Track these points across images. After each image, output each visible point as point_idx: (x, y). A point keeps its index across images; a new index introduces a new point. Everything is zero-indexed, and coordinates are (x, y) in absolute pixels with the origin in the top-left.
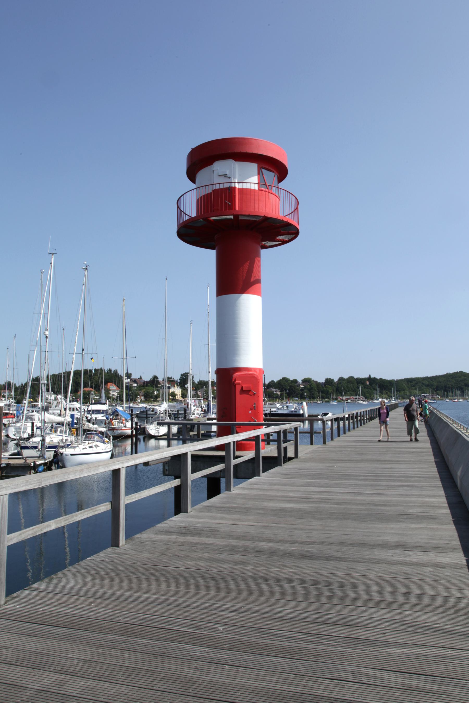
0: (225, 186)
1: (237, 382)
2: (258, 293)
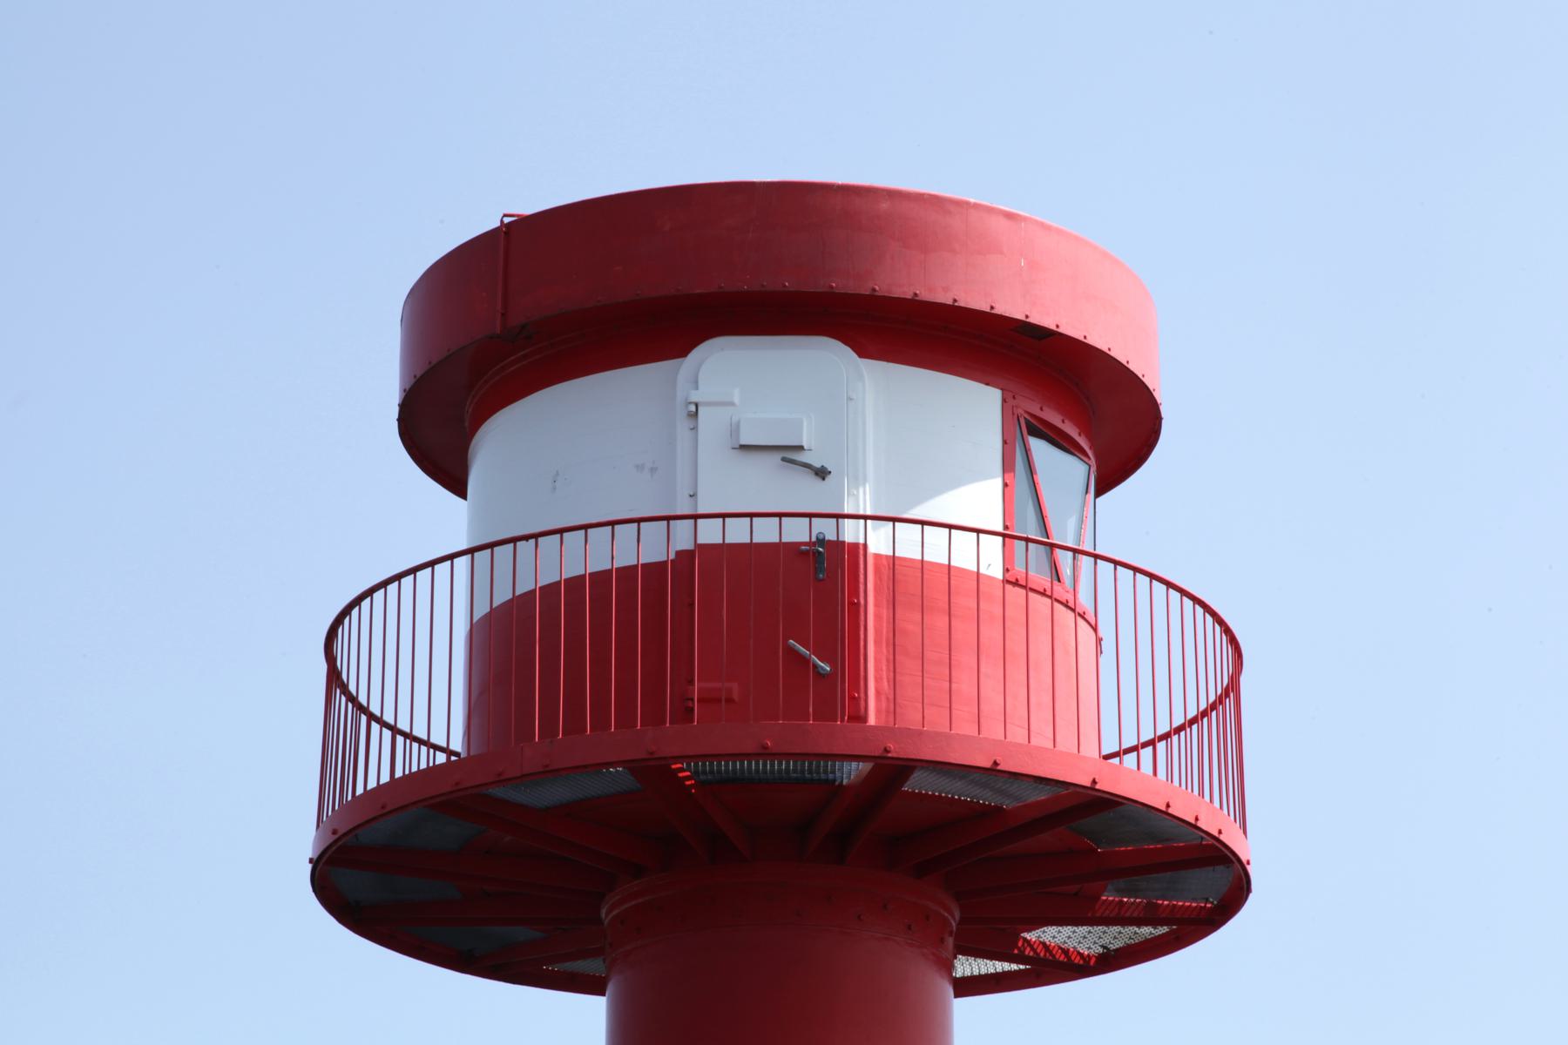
0: (796, 532)
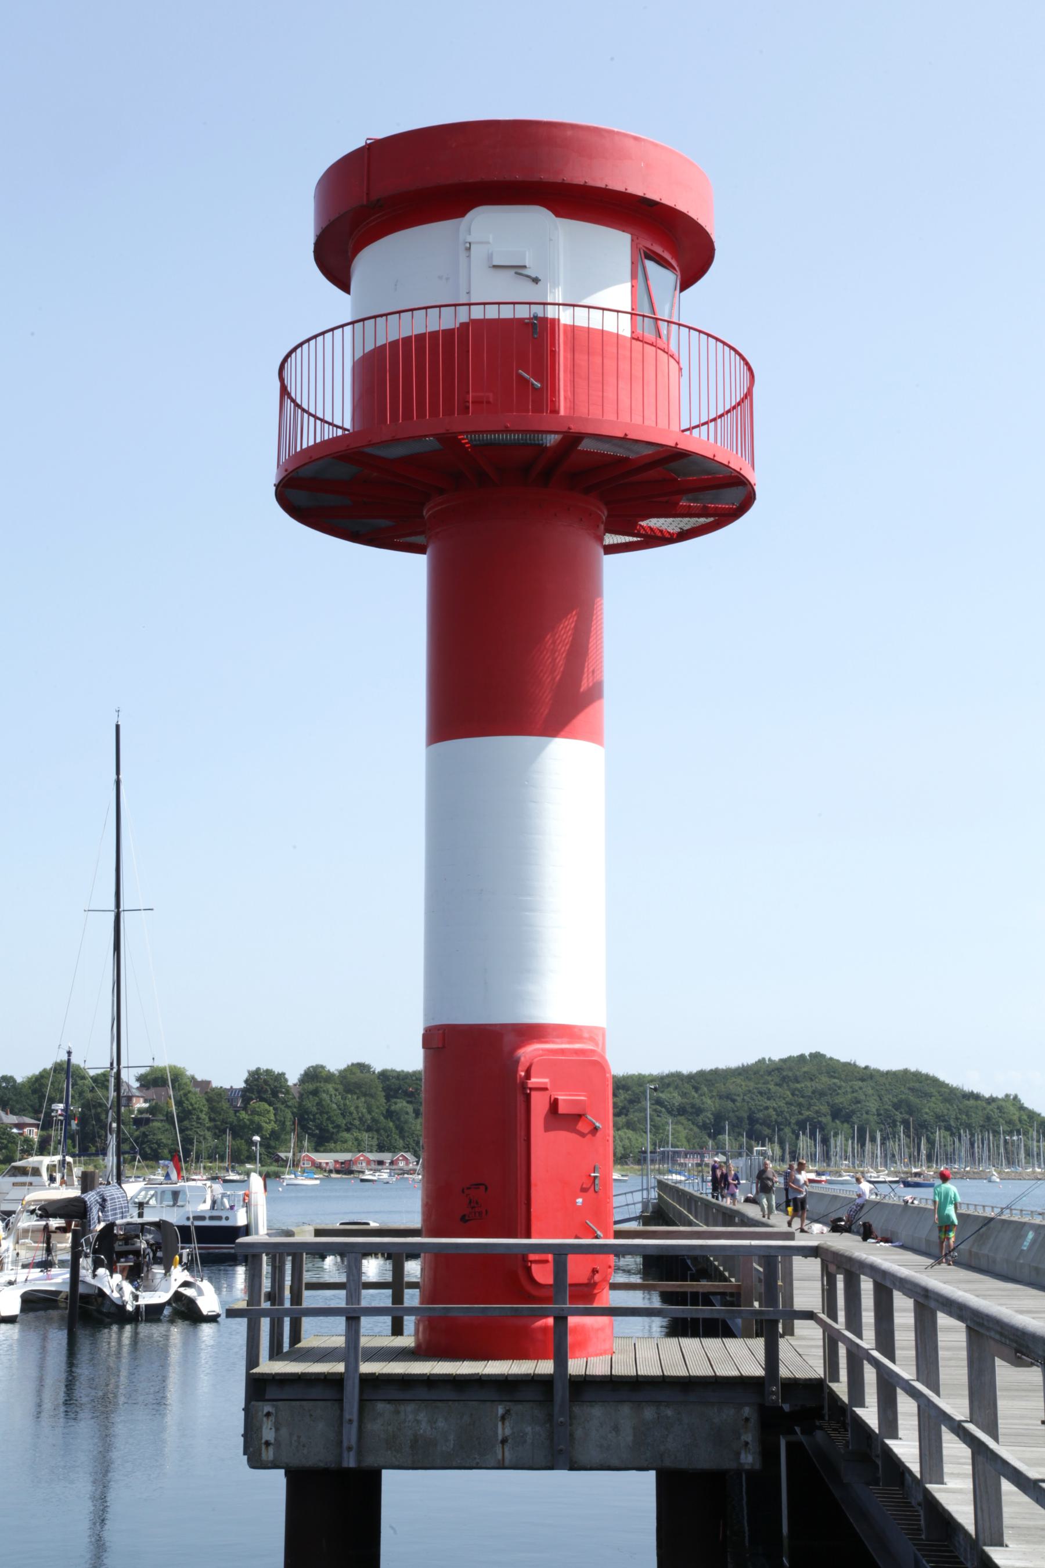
1: (534, 1081)
2: (594, 735)
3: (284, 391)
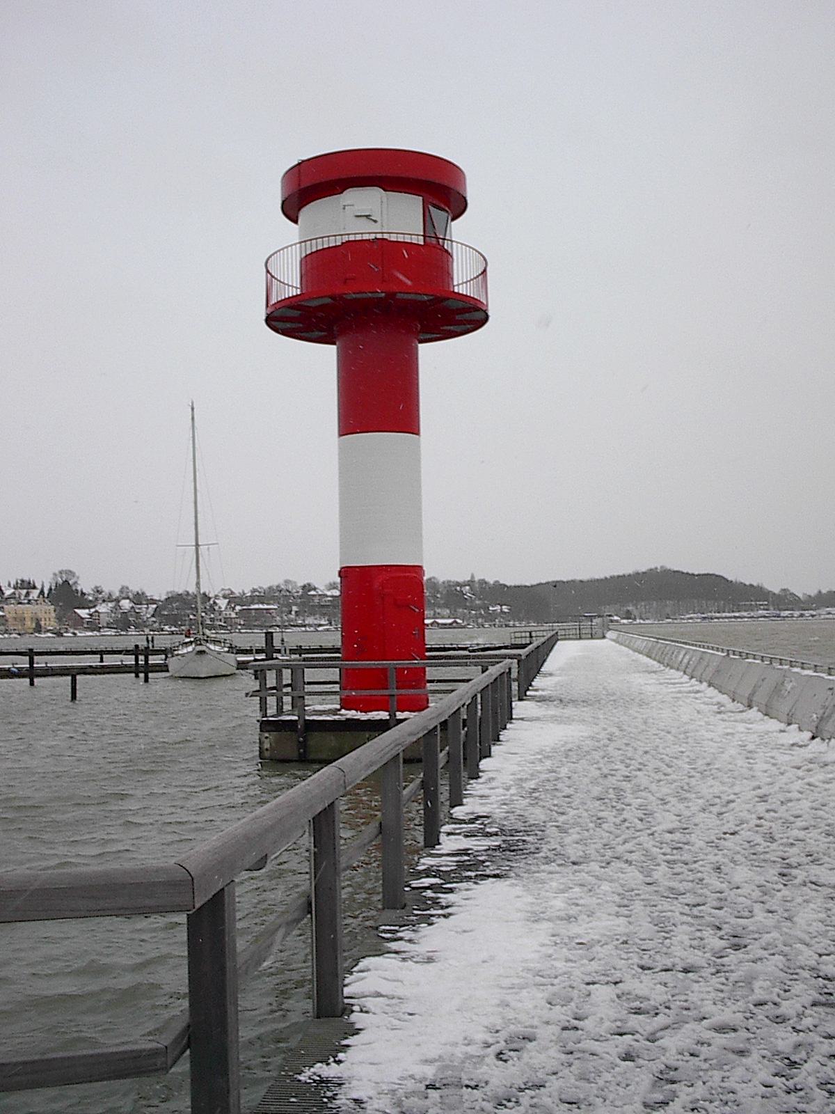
3: (268, 271)
